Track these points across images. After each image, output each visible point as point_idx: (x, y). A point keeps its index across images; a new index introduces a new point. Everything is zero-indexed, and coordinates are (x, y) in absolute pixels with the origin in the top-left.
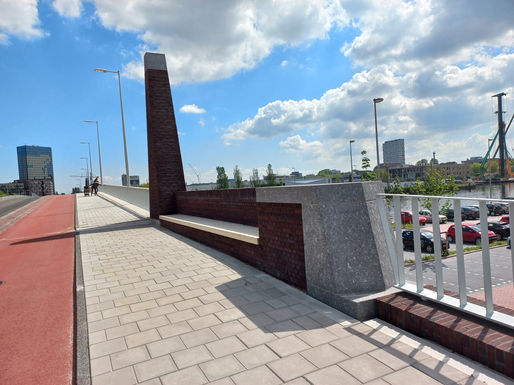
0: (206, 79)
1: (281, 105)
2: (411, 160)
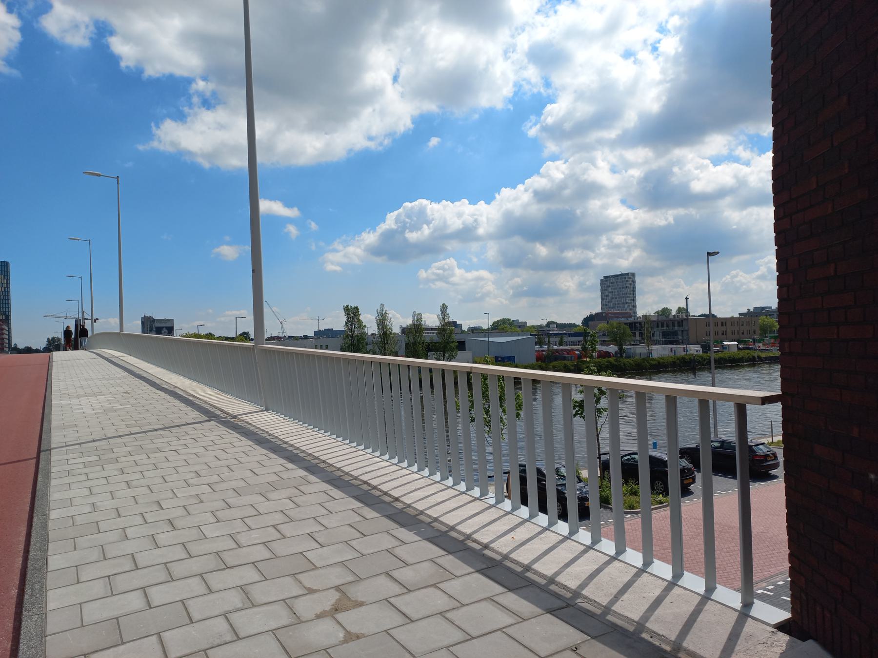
0: (302, 161)
1: (429, 211)
2: (647, 305)
